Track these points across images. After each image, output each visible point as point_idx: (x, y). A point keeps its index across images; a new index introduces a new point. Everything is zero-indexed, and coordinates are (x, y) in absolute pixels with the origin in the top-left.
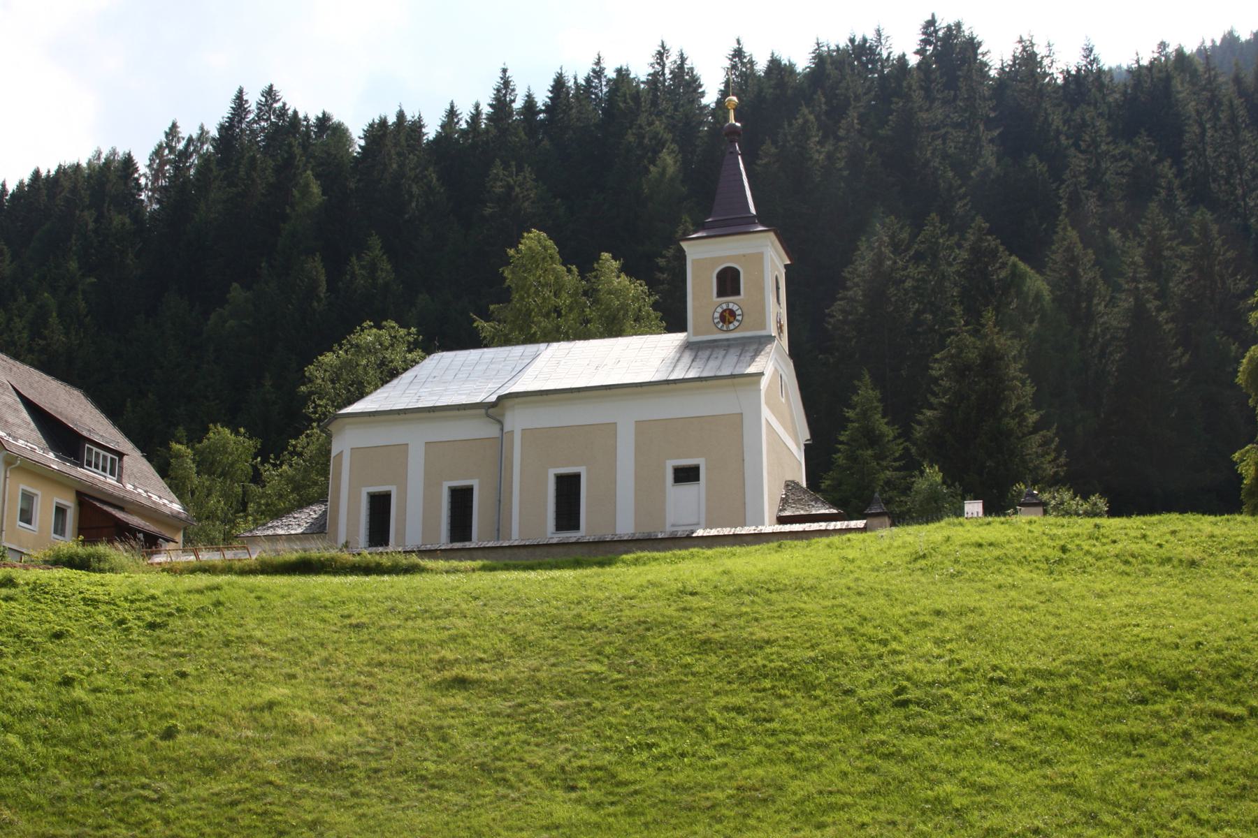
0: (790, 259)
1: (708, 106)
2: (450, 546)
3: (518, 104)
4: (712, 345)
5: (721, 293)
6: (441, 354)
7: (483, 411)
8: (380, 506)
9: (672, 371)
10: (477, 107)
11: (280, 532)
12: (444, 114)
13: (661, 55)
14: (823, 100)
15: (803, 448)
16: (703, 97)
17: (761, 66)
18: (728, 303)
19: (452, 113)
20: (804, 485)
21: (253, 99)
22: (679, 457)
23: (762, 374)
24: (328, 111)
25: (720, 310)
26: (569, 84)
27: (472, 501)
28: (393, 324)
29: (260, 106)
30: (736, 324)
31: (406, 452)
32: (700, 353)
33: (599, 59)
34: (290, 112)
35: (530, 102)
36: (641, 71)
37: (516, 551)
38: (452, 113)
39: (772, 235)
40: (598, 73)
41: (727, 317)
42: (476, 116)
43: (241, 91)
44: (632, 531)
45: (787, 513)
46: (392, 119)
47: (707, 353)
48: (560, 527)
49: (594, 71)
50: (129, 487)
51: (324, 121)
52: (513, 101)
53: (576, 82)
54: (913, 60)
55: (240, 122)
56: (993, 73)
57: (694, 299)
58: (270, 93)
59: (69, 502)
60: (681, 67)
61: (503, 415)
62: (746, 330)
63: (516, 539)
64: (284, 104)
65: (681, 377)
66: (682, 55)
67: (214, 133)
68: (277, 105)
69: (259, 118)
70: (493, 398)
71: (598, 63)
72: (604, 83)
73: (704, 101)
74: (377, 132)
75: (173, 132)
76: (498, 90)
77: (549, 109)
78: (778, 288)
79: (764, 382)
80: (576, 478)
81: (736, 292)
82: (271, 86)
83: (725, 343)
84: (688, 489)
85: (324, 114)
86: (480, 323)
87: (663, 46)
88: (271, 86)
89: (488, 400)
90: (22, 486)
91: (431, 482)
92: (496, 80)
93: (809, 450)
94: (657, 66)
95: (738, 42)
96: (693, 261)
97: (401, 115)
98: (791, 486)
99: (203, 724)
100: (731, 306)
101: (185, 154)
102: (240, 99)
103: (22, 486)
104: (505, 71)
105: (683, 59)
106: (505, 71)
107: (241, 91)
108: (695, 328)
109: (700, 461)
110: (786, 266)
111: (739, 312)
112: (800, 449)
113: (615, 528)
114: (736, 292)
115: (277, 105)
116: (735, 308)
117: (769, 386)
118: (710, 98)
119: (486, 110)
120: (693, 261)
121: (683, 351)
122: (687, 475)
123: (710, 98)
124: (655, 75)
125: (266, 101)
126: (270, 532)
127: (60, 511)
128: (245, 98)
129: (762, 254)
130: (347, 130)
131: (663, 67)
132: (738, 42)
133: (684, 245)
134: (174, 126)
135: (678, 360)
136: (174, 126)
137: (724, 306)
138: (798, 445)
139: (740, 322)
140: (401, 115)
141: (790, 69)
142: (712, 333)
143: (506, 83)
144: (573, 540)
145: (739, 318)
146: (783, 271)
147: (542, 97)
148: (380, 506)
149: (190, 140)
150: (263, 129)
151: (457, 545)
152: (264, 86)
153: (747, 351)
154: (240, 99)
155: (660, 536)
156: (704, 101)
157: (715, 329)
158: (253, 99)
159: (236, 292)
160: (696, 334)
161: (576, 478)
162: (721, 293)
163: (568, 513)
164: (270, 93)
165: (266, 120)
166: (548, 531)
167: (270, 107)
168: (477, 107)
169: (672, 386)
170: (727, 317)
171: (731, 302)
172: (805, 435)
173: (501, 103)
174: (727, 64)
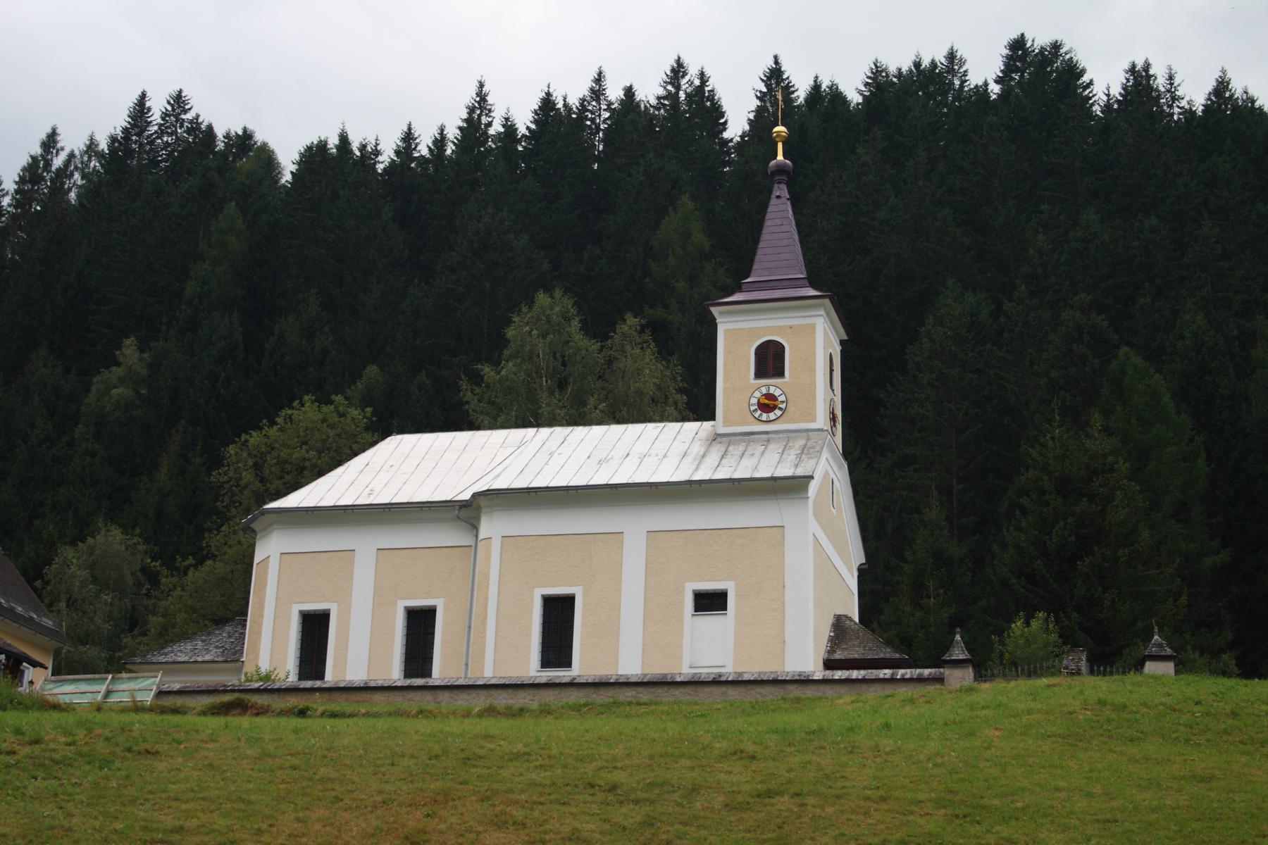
0: (848, 334)
1: (731, 140)
2: (408, 682)
3: (497, 128)
5: (760, 373)
6: (400, 437)
9: (697, 469)
10: (442, 130)
11: (182, 658)
13: (678, 71)
15: (856, 574)
16: (725, 129)
17: (801, 93)
18: (769, 386)
19: (409, 137)
20: (857, 620)
21: (158, 106)
22: (701, 580)
23: (811, 477)
24: (250, 127)
25: (757, 394)
26: (558, 106)
27: (434, 626)
29: (165, 115)
30: (778, 412)
32: (731, 448)
34: (203, 127)
35: (510, 128)
36: (650, 91)
39: (827, 301)
40: (597, 92)
41: (769, 403)
42: (440, 142)
43: (143, 96)
44: (639, 672)
45: (838, 655)
46: (333, 141)
47: (741, 448)
48: (546, 663)
49: (592, 90)
51: (245, 140)
52: (489, 124)
53: (566, 105)
54: (995, 89)
55: (139, 134)
56: (1097, 109)
57: (725, 380)
58: (179, 102)
62: (789, 421)
63: (489, 673)
64: (198, 116)
65: (707, 478)
67: (103, 146)
68: (189, 116)
69: (161, 132)
70: (466, 496)
72: (604, 107)
73: (726, 135)
74: (315, 156)
75: (50, 143)
76: (471, 110)
77: (533, 135)
78: (832, 371)
79: (813, 487)
80: (569, 601)
81: (780, 373)
82: (180, 91)
83: (429, 505)
84: (710, 622)
85: (245, 130)
88: (180, 91)
89: (456, 499)
91: (381, 598)
92: (469, 96)
93: (863, 573)
94: (669, 87)
97: (344, 140)
98: (839, 624)
99: (855, 784)
100: (772, 390)
101: (64, 173)
104: (481, 85)
106: (481, 85)
107: (143, 96)
108: (725, 417)
109: (729, 586)
110: (842, 343)
111: (782, 398)
112: (853, 577)
113: (617, 670)
114: (780, 373)
115: (189, 116)
116: (777, 393)
117: (818, 494)
118: (736, 126)
119: (452, 133)
121: (710, 445)
122: (710, 602)
123: (736, 126)
124: (669, 96)
125: (173, 110)
128: (148, 104)
129: (815, 324)
130: (273, 152)
131: (678, 88)
132: (776, 62)
133: (715, 310)
135: (704, 456)
137: (764, 391)
138: (850, 571)
139: (752, 412)
140: (344, 140)
141: (836, 96)
142: (747, 424)
143: (482, 97)
144: (567, 680)
146: (838, 348)
147: (524, 122)
149: (72, 155)
150: (167, 144)
151: (308, 684)
152: (172, 89)
153: (791, 448)
155: (679, 679)
156: (726, 135)
157: (752, 419)
158: (158, 106)
159: (129, 351)
160: (726, 424)
161: (569, 601)
162: (760, 373)
164: (179, 102)
165: (170, 135)
166: (530, 667)
167: (177, 117)
168: (442, 130)
171: (773, 386)
172: (857, 556)
173: (473, 127)
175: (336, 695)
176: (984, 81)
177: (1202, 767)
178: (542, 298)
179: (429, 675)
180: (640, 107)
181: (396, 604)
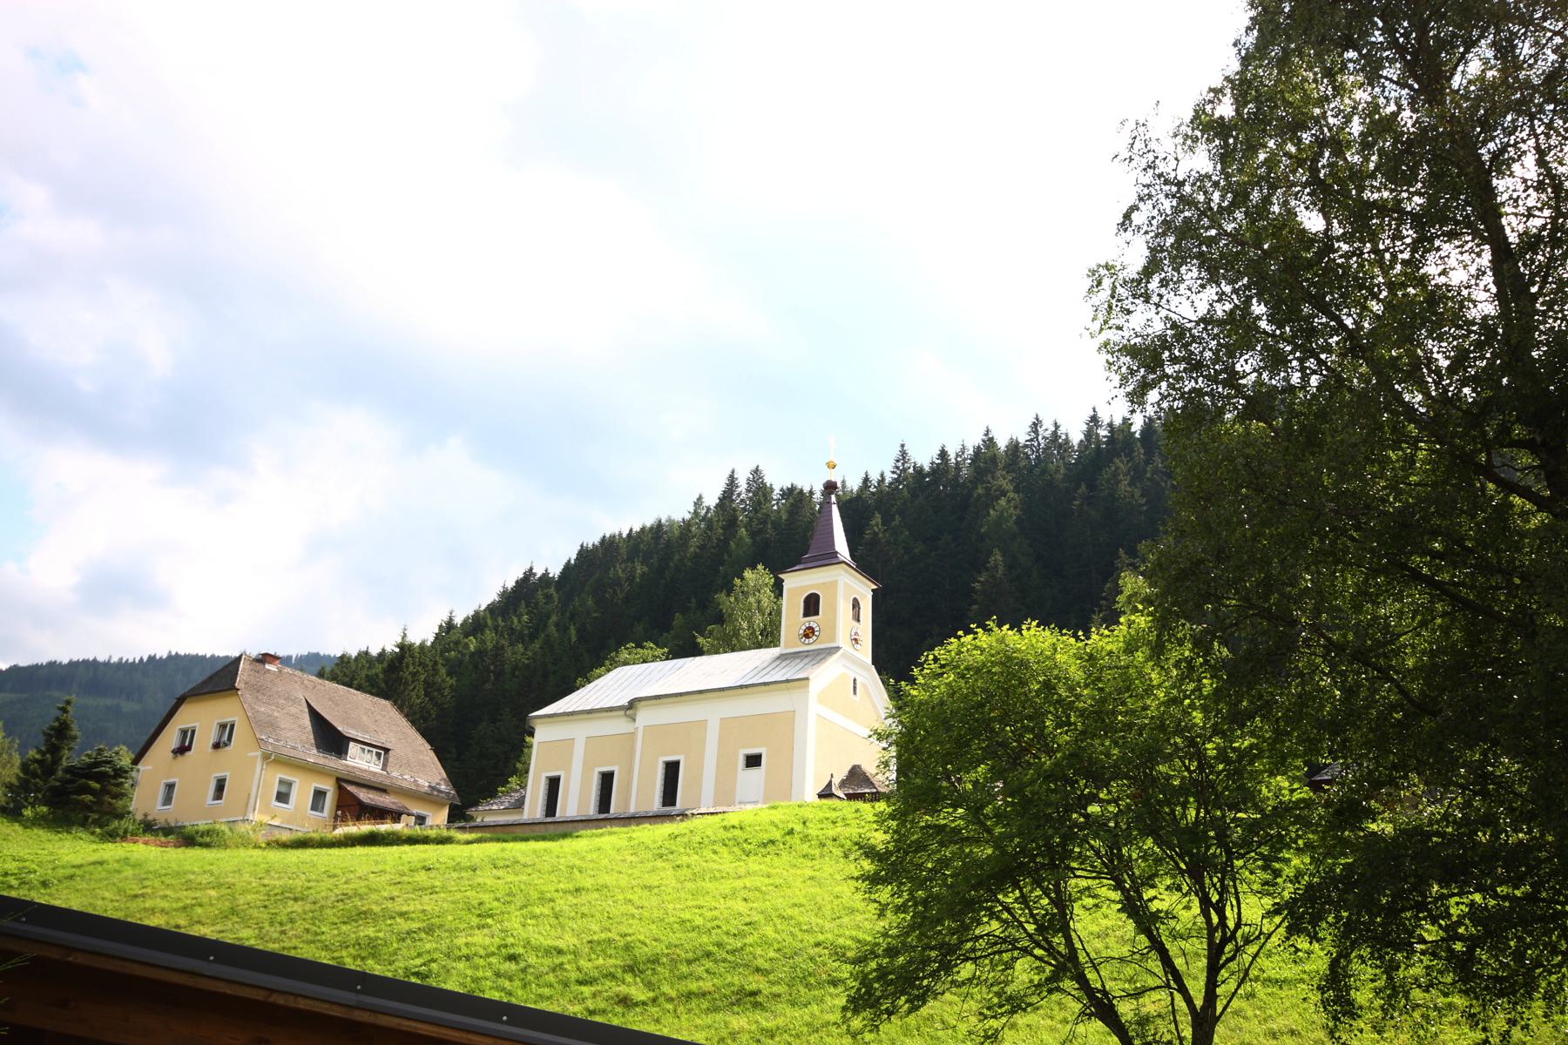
4: (796, 655)
5: (806, 614)
7: (623, 712)
8: (554, 783)
11: (495, 807)
12: (861, 481)
13: (1036, 425)
14: (1142, 451)
24: (795, 483)
25: (804, 628)
28: (652, 645)
30: (815, 638)
31: (573, 744)
33: (988, 431)
37: (576, 824)
38: (866, 480)
41: (809, 633)
43: (733, 472)
44: (575, 814)
48: (664, 805)
50: (395, 774)
59: (329, 786)
60: (1055, 433)
61: (635, 715)
62: (820, 643)
66: (1056, 423)
71: (986, 435)
81: (817, 613)
84: (754, 772)
86: (700, 640)
87: (1037, 419)
90: (280, 775)
92: (896, 453)
95: (1094, 410)
96: (788, 589)
102: (732, 480)
103: (280, 775)
104: (903, 446)
105: (1057, 426)
106: (903, 446)
107: (733, 472)
111: (817, 629)
114: (817, 613)
120: (788, 589)
122: (753, 761)
126: (487, 808)
127: (319, 795)
129: (836, 581)
132: (1094, 410)
134: (700, 498)
136: (700, 498)
139: (818, 636)
145: (817, 633)
148: (554, 783)
151: (602, 816)
154: (732, 480)
160: (786, 647)
162: (806, 614)
163: (669, 795)
169: (745, 690)
170: (809, 633)
171: (812, 621)
173: (901, 473)
174: (1085, 427)
175: (498, 829)
176: (446, 619)
177: (509, 880)
178: (1407, 400)
179: (608, 812)
180: (56, 787)
181: (296, 808)
